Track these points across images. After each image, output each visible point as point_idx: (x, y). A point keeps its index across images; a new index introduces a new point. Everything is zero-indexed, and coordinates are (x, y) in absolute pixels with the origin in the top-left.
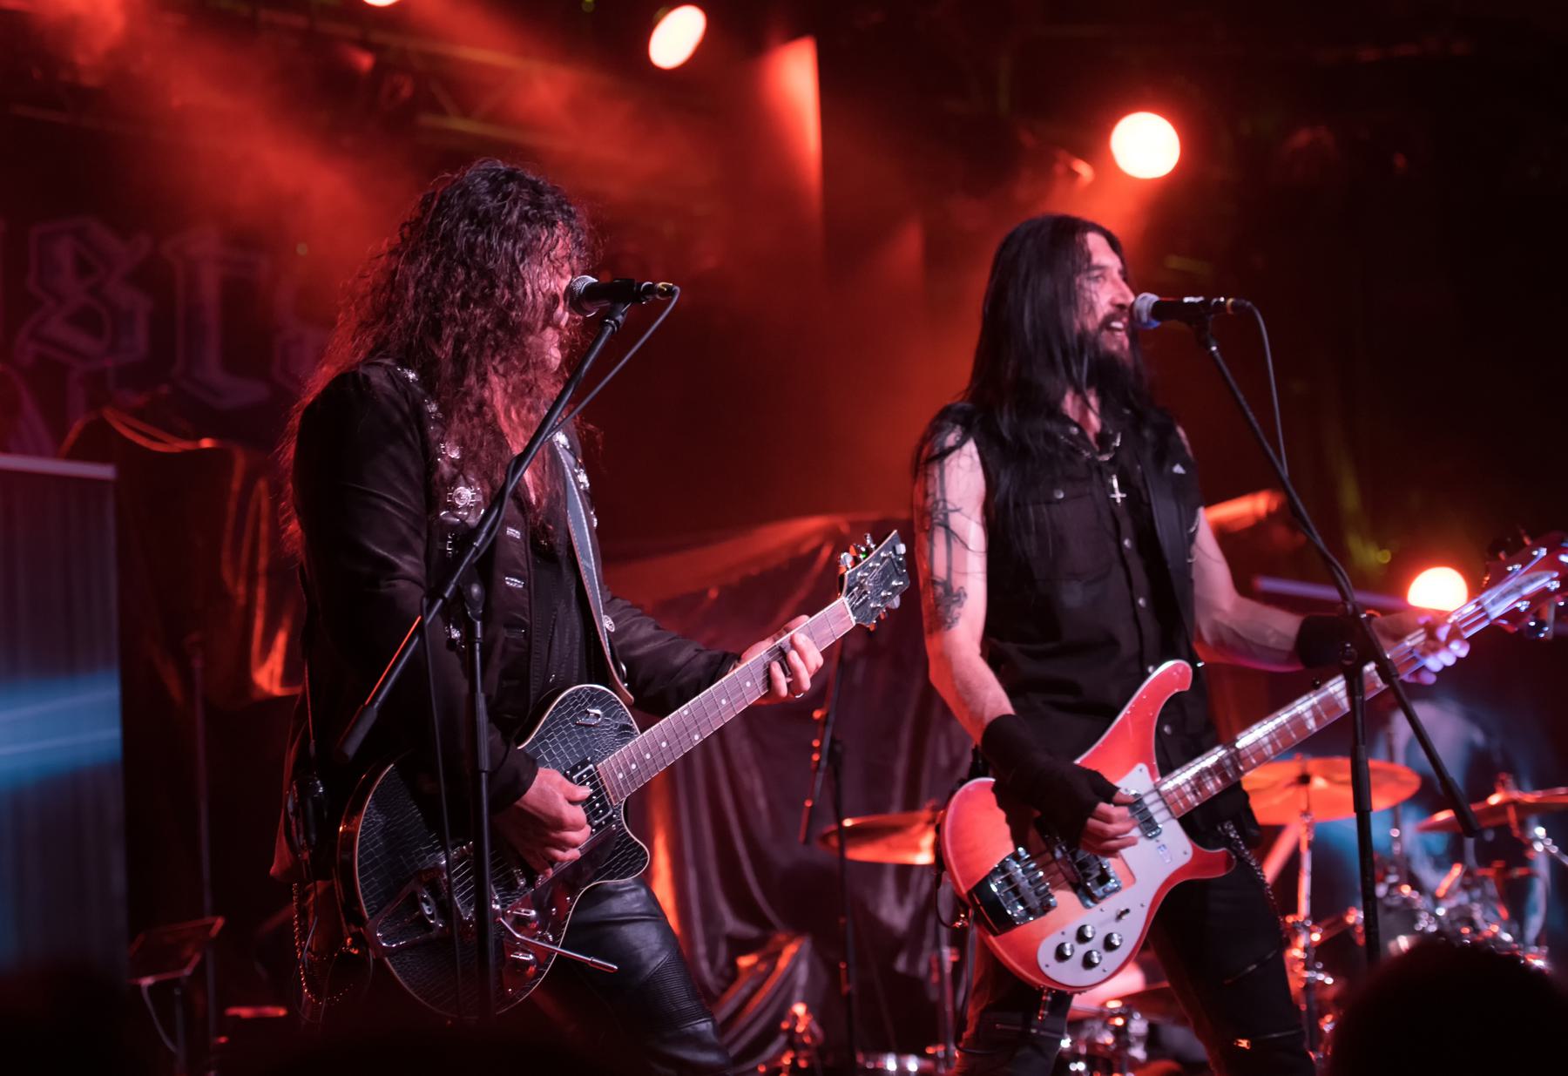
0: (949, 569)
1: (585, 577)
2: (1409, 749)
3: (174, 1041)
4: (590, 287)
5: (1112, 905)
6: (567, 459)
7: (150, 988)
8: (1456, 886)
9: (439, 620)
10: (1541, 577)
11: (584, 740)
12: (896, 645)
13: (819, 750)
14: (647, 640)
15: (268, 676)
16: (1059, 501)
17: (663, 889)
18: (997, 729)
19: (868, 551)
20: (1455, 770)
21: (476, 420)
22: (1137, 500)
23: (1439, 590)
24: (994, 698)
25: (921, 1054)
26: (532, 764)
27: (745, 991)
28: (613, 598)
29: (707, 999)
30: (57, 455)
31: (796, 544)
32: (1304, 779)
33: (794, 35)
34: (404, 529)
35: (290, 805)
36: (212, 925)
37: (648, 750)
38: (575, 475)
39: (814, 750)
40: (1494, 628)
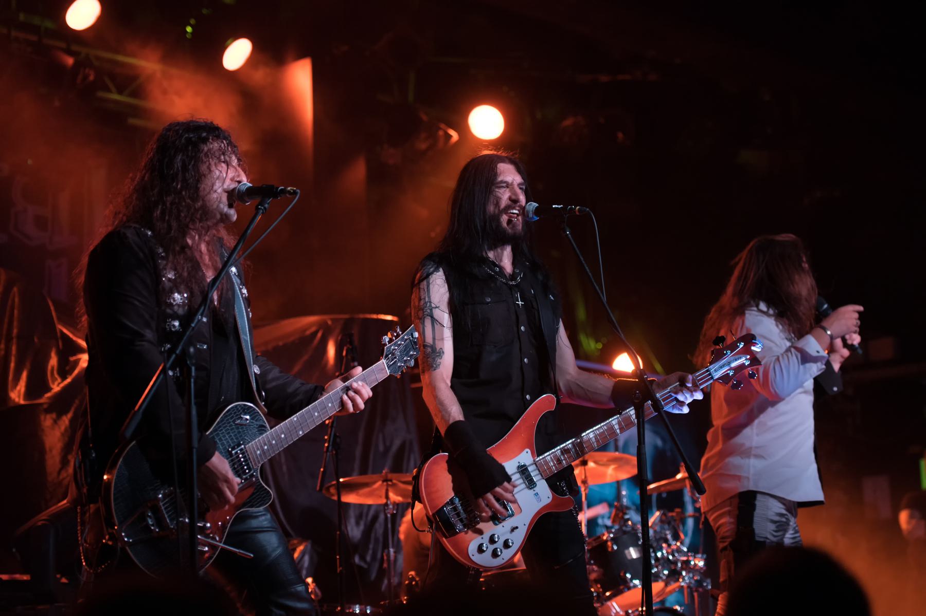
0: (434, 339)
1: (243, 344)
5: (509, 523)
6: (236, 280)
19: (398, 336)
24: (455, 412)
33: (300, 56)
37: (273, 439)
38: (240, 289)
39: (325, 441)
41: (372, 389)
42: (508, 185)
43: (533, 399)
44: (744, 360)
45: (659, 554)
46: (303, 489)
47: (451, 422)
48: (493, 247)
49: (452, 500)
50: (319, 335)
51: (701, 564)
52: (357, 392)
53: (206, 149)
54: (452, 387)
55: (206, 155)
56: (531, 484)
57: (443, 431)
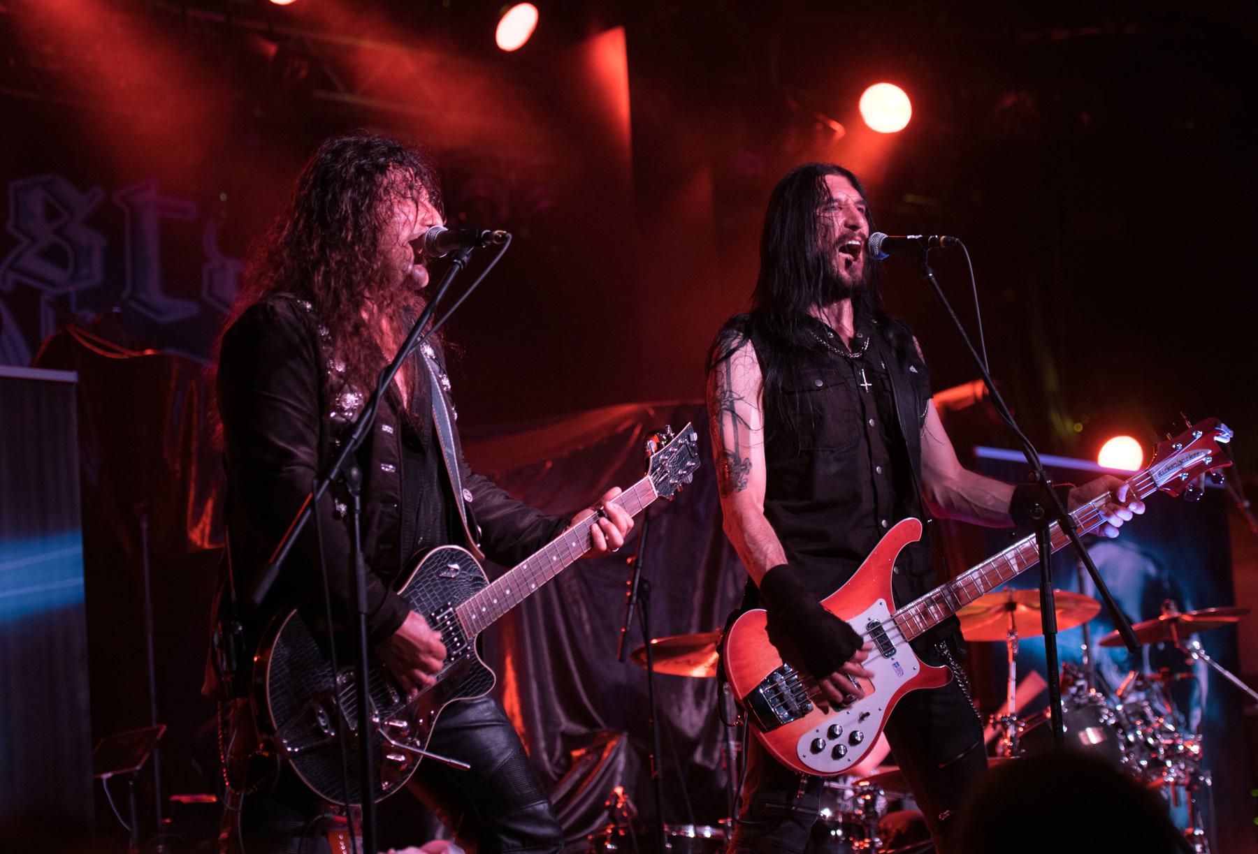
0: (737, 444)
1: (447, 461)
3: (128, 821)
5: (858, 707)
6: (432, 367)
7: (108, 779)
8: (1130, 688)
9: (329, 496)
10: (1198, 454)
11: (446, 589)
13: (631, 588)
14: (499, 507)
15: (199, 535)
16: (819, 389)
17: (511, 701)
19: (669, 439)
21: (356, 340)
22: (879, 391)
23: (1121, 454)
25: (714, 825)
26: (406, 606)
27: (577, 776)
28: (473, 473)
29: (545, 785)
30: (33, 365)
32: (1011, 606)
33: (608, 26)
34: (300, 426)
35: (216, 639)
36: (158, 730)
38: (439, 380)
40: (1160, 494)
42: (842, 207)
43: (890, 526)
44: (1204, 457)
45: (1131, 738)
46: (594, 658)
47: (768, 567)
48: (827, 302)
50: (637, 431)
51: (1195, 749)
52: (611, 518)
53: (385, 182)
54: (765, 514)
55: (387, 191)
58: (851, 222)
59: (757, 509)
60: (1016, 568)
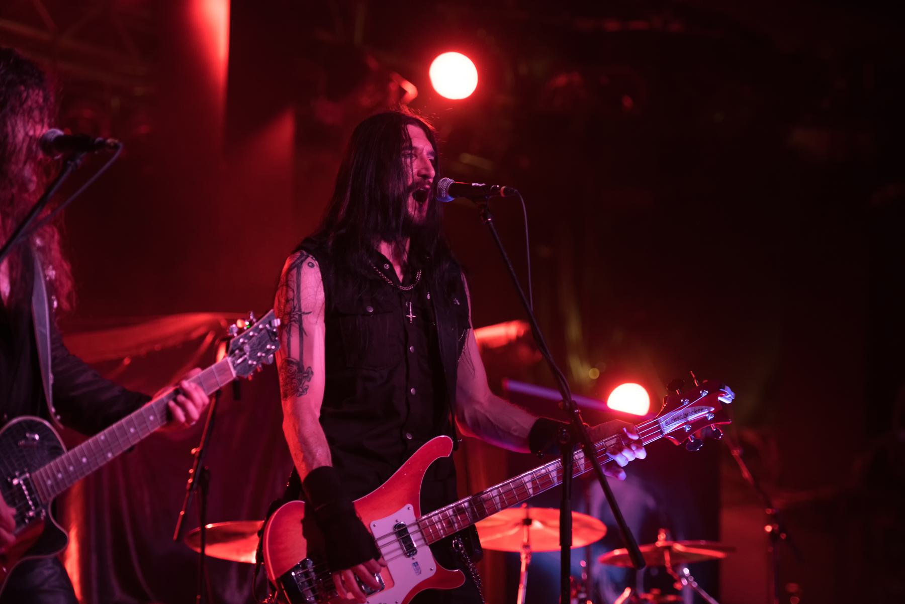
0: (301, 354)
2: (603, 508)
4: (59, 138)
10: (702, 410)
12: (259, 396)
17: (72, 567)
18: (318, 474)
20: (632, 522)
24: (322, 455)
31: (188, 332)
32: (528, 522)
41: (210, 397)
44: (705, 413)
47: (315, 466)
49: (304, 563)
52: (188, 395)
54: (321, 420)
56: (410, 550)
57: (303, 474)
58: (424, 172)
59: (313, 415)
60: (531, 491)
